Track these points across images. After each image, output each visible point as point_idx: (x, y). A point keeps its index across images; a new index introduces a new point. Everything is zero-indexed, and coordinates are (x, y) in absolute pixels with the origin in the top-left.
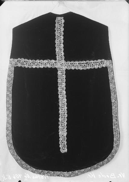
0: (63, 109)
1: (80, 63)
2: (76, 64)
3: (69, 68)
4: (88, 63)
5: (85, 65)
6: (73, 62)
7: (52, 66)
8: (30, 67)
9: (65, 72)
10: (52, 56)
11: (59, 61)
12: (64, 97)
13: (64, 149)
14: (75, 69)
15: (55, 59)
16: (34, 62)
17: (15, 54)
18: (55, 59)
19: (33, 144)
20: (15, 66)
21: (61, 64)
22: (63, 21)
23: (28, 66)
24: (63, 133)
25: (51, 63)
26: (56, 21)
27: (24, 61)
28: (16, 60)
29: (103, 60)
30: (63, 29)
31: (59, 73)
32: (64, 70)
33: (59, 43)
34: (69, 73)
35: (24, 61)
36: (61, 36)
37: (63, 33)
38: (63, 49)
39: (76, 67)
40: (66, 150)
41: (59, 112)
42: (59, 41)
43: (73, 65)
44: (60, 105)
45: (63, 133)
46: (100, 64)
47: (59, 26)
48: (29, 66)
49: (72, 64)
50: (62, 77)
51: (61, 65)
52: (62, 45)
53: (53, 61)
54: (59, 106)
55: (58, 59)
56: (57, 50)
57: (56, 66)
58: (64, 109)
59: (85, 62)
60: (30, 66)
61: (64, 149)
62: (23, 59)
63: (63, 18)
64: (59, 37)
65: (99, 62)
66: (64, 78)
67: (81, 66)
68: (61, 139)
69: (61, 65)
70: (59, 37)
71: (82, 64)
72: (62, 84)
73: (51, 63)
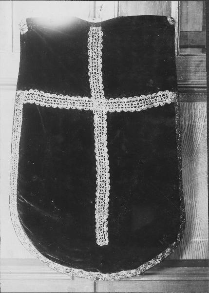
0: (104, 176)
1: (131, 101)
2: (124, 102)
3: (112, 111)
4: (143, 99)
5: (138, 104)
6: (118, 100)
7: (84, 108)
8: (48, 106)
9: (105, 118)
10: (84, 90)
11: (96, 98)
12: (106, 158)
13: (102, 239)
14: (123, 111)
15: (90, 96)
16: (54, 98)
17: (24, 83)
18: (90, 96)
19: (53, 215)
20: (25, 102)
21: (99, 103)
22: (101, 34)
23: (45, 104)
24: (101, 215)
25: (82, 102)
26: (90, 34)
27: (39, 95)
28: (26, 92)
29: (167, 92)
30: (101, 47)
31: (96, 119)
32: (104, 114)
33: (100, 133)
34: (114, 119)
35: (39, 95)
36: (105, 161)
37: (101, 53)
38: (101, 80)
39: (124, 108)
40: (107, 242)
41: (97, 182)
42: (95, 66)
43: (119, 105)
44: (99, 171)
45: (101, 215)
46: (162, 99)
47: (102, 183)
48: (46, 104)
49: (118, 102)
50: (101, 125)
51: (99, 105)
52: (100, 73)
53: (86, 98)
54: (96, 172)
55: (93, 95)
56: (91, 80)
57: (90, 108)
58: (101, 114)
59: (138, 98)
60: (48, 104)
61: (102, 239)
62: (37, 90)
63: (100, 28)
64: (95, 59)
65: (160, 96)
66: (105, 126)
67: (133, 106)
68: (98, 225)
69: (99, 105)
70: (95, 59)
71: (134, 101)
72: (101, 136)
73: (82, 102)
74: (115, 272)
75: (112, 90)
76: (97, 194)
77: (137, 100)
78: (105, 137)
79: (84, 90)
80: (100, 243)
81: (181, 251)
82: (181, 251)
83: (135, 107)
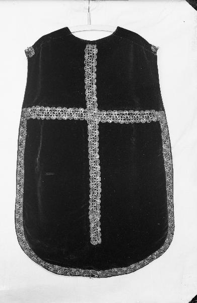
10: (81, 102)
13: (96, 238)
15: (85, 107)
18: (85, 107)
20: (28, 118)
24: (95, 217)
31: (90, 127)
34: (104, 127)
40: (100, 241)
45: (95, 217)
51: (94, 116)
52: (95, 86)
59: (127, 112)
61: (96, 238)
63: (95, 46)
69: (94, 116)
74: (108, 268)
75: (103, 105)
76: (90, 196)
77: (126, 114)
78: (97, 144)
79: (81, 102)
80: (94, 243)
81: (26, 232)
82: (26, 232)
83: (125, 120)
